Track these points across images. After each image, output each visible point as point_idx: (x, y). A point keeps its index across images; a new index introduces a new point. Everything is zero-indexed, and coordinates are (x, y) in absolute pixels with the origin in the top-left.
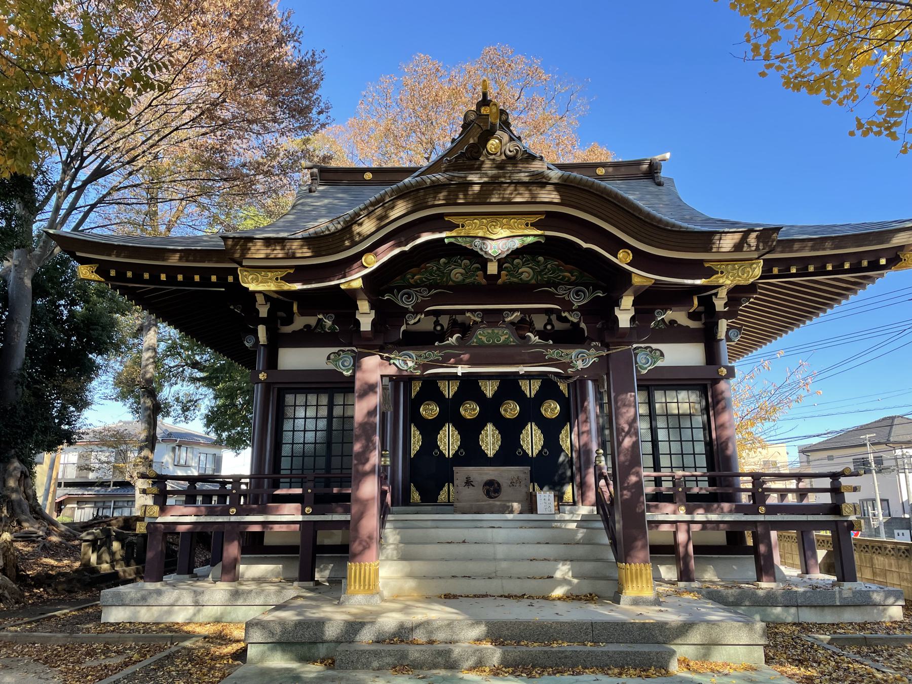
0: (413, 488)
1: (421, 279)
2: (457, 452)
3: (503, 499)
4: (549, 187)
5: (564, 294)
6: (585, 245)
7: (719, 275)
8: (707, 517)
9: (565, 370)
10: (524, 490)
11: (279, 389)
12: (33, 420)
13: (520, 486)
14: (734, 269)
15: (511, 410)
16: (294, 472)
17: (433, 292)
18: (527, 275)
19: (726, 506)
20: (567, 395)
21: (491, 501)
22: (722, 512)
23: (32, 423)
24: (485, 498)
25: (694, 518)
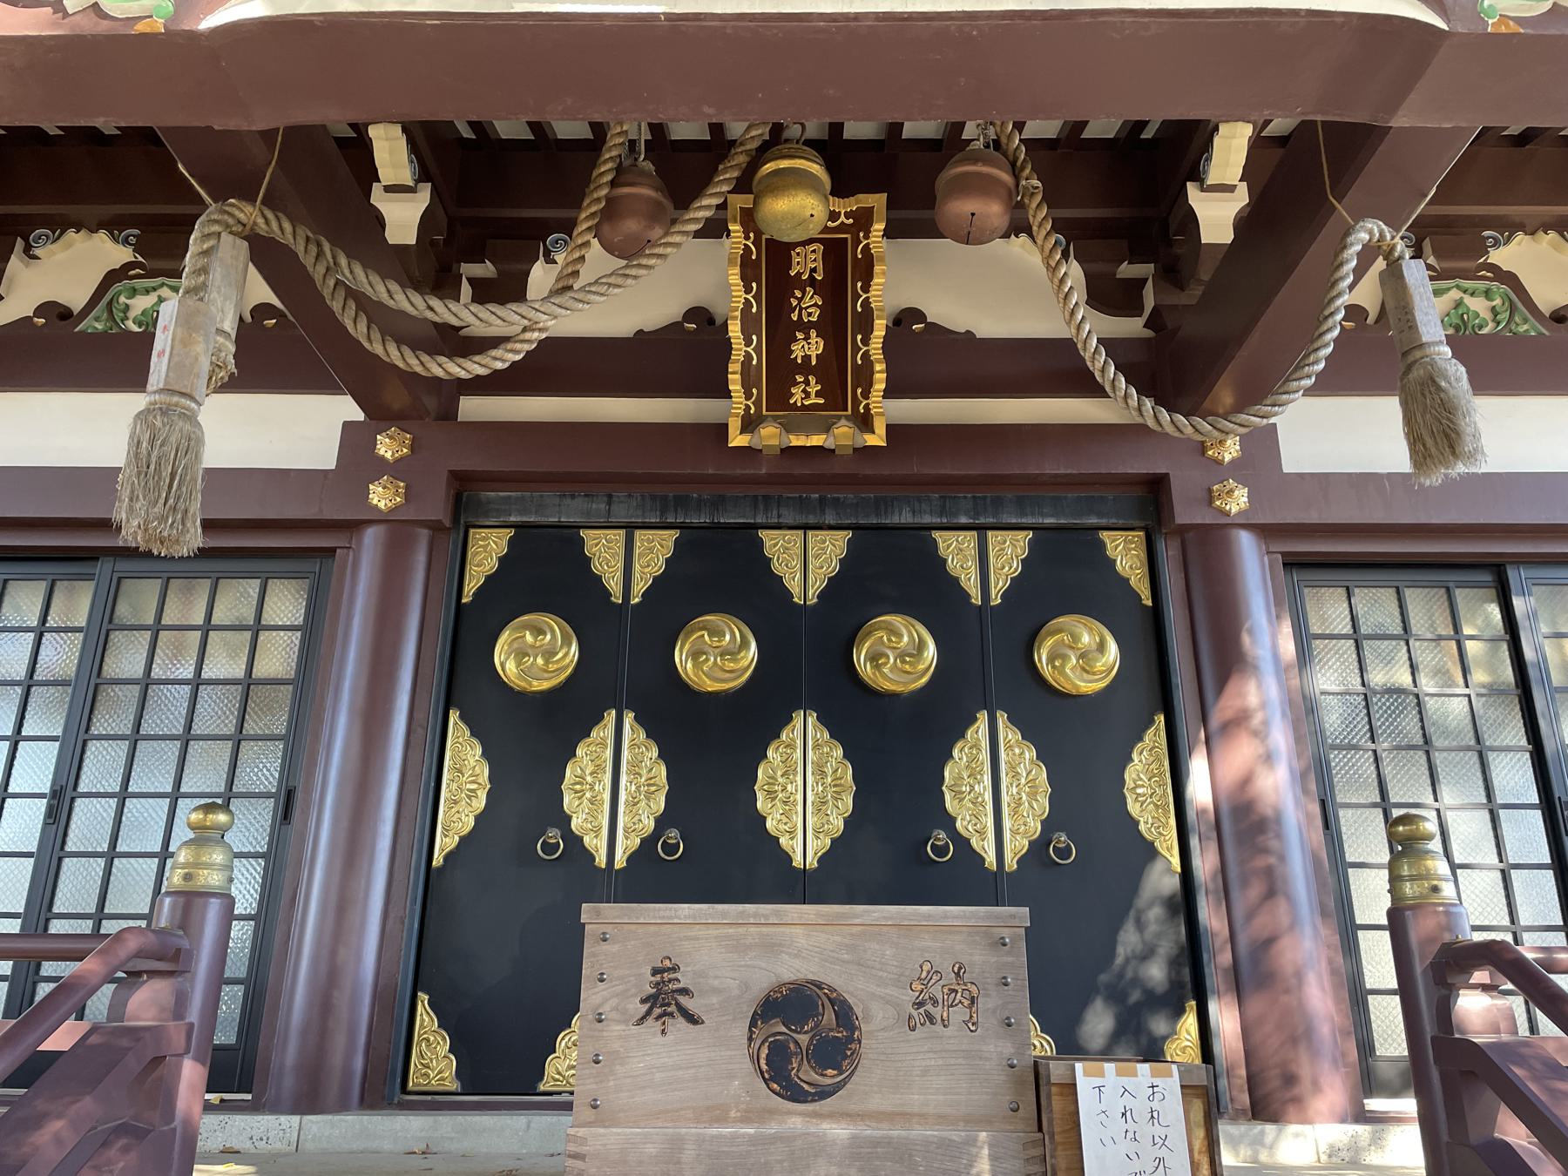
0: (426, 1018)
2: (648, 843)
10: (997, 1048)
13: (971, 1023)
15: (902, 656)
21: (795, 1120)
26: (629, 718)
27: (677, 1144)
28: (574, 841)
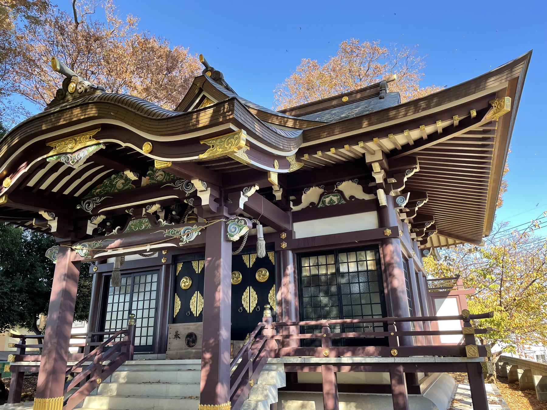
1: (100, 192)
2: (255, 308)
4: (90, 106)
7: (211, 148)
8: (353, 360)
9: (178, 244)
11: (105, 276)
16: (111, 330)
17: (103, 199)
18: (161, 177)
19: (371, 349)
20: (274, 264)
21: (190, 350)
22: (369, 355)
24: (187, 347)
25: (340, 360)
27: (177, 353)
28: (191, 312)
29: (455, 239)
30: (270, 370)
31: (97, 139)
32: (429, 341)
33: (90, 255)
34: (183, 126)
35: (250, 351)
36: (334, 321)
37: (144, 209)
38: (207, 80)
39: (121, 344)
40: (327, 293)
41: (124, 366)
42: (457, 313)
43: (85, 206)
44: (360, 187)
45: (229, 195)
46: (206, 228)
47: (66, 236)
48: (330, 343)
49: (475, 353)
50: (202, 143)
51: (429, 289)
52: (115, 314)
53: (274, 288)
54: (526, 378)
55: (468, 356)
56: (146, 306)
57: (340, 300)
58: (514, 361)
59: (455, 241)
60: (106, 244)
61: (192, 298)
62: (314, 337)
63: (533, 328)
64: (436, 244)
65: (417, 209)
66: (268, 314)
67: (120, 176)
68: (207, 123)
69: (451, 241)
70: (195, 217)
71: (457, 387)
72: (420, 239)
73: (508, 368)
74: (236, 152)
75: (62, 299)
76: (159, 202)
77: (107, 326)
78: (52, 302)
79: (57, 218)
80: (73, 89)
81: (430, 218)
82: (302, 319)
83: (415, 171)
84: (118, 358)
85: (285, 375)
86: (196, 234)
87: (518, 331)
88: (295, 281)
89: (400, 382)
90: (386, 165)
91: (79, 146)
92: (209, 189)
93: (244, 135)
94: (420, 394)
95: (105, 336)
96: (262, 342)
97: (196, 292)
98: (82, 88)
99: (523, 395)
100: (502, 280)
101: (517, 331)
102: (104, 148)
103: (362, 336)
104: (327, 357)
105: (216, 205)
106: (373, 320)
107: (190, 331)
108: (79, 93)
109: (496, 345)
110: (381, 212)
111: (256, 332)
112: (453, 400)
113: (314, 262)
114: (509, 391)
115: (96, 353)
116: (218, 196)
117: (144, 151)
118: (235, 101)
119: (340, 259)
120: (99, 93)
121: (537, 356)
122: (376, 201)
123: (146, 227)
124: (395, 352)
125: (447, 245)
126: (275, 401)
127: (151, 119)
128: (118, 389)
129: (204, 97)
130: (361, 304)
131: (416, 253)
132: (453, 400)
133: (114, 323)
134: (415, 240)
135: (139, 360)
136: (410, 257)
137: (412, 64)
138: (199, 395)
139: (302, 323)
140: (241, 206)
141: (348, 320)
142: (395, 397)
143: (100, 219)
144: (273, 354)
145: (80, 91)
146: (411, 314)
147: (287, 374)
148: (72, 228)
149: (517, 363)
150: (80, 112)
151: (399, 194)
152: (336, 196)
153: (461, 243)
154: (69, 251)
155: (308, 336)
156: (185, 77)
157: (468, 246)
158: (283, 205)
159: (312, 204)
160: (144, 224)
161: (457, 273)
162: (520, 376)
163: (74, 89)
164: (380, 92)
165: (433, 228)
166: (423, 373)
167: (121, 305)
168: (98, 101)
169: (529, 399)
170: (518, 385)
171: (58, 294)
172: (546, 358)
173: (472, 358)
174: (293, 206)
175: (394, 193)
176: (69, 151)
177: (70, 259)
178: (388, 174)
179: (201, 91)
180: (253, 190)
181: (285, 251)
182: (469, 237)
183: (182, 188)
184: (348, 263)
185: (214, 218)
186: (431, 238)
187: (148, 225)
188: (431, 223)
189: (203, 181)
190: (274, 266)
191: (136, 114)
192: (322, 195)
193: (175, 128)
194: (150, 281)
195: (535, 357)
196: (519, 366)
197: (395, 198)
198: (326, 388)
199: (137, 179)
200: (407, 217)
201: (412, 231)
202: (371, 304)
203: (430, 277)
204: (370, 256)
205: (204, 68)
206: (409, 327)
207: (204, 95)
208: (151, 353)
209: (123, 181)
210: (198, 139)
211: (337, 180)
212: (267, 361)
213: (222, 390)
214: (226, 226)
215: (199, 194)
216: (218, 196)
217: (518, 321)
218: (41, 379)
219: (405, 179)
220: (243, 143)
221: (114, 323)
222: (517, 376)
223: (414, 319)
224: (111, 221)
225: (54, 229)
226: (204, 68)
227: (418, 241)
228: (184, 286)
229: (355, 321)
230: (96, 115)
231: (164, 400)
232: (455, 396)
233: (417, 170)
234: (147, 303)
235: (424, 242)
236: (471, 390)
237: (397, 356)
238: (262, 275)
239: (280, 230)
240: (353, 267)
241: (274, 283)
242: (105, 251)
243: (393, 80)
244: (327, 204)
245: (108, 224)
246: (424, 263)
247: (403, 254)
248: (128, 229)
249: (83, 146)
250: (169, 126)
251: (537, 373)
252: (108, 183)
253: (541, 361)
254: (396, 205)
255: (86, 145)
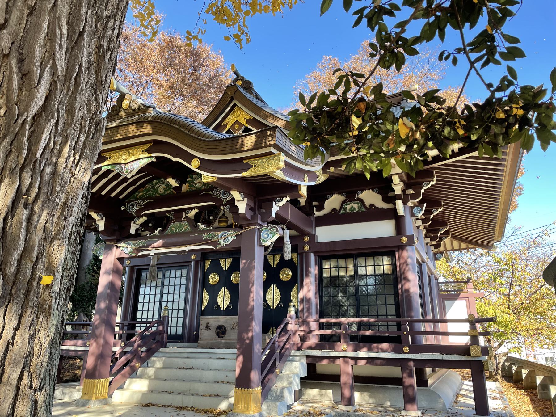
1: (143, 195)
2: (278, 305)
3: (228, 338)
5: (217, 194)
6: (174, 159)
7: (253, 168)
9: (215, 247)
11: (137, 269)
12: (93, 292)
14: (263, 162)
17: (146, 202)
19: (385, 345)
20: (297, 264)
21: (220, 340)
22: (383, 351)
23: (92, 294)
24: (217, 337)
25: (357, 354)
26: (275, 286)
27: (208, 343)
28: (219, 306)
29: (468, 244)
30: (293, 361)
31: (149, 153)
32: (438, 340)
33: (134, 253)
34: (231, 148)
35: (277, 344)
36: (352, 320)
37: (184, 213)
38: (238, 89)
39: (154, 333)
40: (345, 292)
41: (159, 353)
42: (466, 317)
43: (129, 208)
44: (380, 197)
45: (263, 204)
46: (241, 233)
47: (111, 234)
48: (348, 340)
49: (478, 353)
50: (245, 162)
51: (442, 291)
52: (146, 305)
53: (296, 287)
54: (530, 378)
55: (472, 355)
56: (176, 298)
57: (357, 300)
58: (521, 362)
59: (467, 246)
60: (150, 243)
61: (220, 293)
62: (333, 333)
63: (538, 331)
64: (449, 247)
65: (432, 216)
66: (292, 311)
67: (161, 181)
68: (251, 147)
69: (463, 245)
70: (226, 219)
71: (463, 383)
72: (434, 243)
73: (514, 368)
74: (275, 172)
75: (109, 291)
76: (198, 208)
77: (139, 315)
78: (101, 293)
79: (104, 218)
80: (126, 106)
81: (444, 224)
82: (321, 317)
83: (432, 183)
84: (154, 346)
85: (306, 366)
86: (233, 238)
87: (524, 333)
88: (316, 281)
89: (411, 376)
90: (405, 178)
91: (133, 158)
92: (246, 199)
93: (283, 157)
94: (428, 386)
95: (137, 325)
96: (287, 336)
97: (223, 287)
98: (135, 105)
99: (526, 394)
100: (511, 284)
101: (523, 334)
102: (155, 160)
103: (378, 334)
104: (346, 351)
105: (252, 213)
106: (387, 320)
107: (220, 324)
108: (132, 110)
109: (503, 347)
110: (399, 221)
111: (282, 326)
112: (458, 395)
113: (334, 264)
114: (513, 390)
115: (136, 340)
116: (253, 206)
117: (192, 166)
118: (277, 129)
119: (358, 263)
120: (151, 112)
121: (546, 358)
122: (395, 210)
123: (185, 230)
124: (406, 349)
125: (460, 249)
126: (298, 388)
127: (201, 140)
128: (155, 373)
129: (235, 105)
130: (377, 305)
131: (429, 258)
132: (458, 395)
133: (145, 313)
134: (429, 245)
135: (172, 348)
136: (423, 262)
137: (433, 64)
138: (234, 381)
139: (323, 320)
140: (273, 215)
141: (365, 319)
142: (406, 389)
143: (142, 220)
144: (295, 348)
145: (133, 108)
146: (423, 317)
147: (309, 365)
148: (116, 228)
149: (522, 364)
150: (135, 129)
151: (417, 204)
152: (357, 204)
153: (473, 248)
154: (115, 248)
155: (328, 332)
156: (210, 76)
157: (479, 251)
158: (307, 211)
159: (334, 210)
160: (184, 226)
161: (469, 275)
162: (524, 376)
163: (128, 106)
164: (402, 102)
165: (447, 233)
166: (431, 369)
167: (152, 297)
168: (152, 120)
169: (531, 397)
170: (522, 384)
171: (106, 286)
172: (555, 360)
173: (475, 357)
174: (317, 211)
175: (411, 203)
176: (123, 162)
177: (115, 256)
178: (407, 186)
179: (232, 99)
180: (284, 201)
181: (307, 253)
182: (481, 242)
183: (219, 196)
184: (366, 266)
185: (249, 225)
186: (444, 243)
187: (187, 228)
188: (445, 229)
189: (241, 192)
190: (297, 267)
191: (187, 134)
192: (343, 203)
193: (224, 149)
194: (180, 276)
195: (544, 359)
196: (524, 367)
197: (412, 208)
198: (344, 379)
199: (178, 185)
200: (423, 223)
201: (426, 236)
202: (386, 305)
203: (441, 279)
204: (386, 261)
205: (235, 76)
206: (420, 328)
207: (235, 103)
208: (180, 342)
209: (164, 186)
210: (241, 160)
211: (358, 189)
212: (290, 353)
213: (255, 376)
214: (260, 233)
215: (236, 203)
216: (253, 206)
217: (524, 324)
218: (90, 362)
219: (422, 191)
220: (282, 165)
221: (145, 313)
222: (522, 376)
223: (425, 321)
224: (153, 222)
225: (101, 228)
226: (235, 76)
227: (432, 245)
228: (212, 282)
229: (372, 320)
230: (150, 132)
231: (199, 384)
232: (460, 391)
233: (435, 182)
234: (176, 296)
235: (437, 246)
236: (473, 386)
237: (408, 353)
238: (286, 275)
239: (303, 234)
240: (370, 270)
241: (297, 282)
242: (148, 250)
243: (415, 90)
244: (348, 211)
245: (150, 225)
246: (437, 265)
247: (417, 260)
248: (169, 230)
249: (136, 158)
250: (218, 147)
251: (540, 373)
252: (150, 187)
253: (550, 364)
254: (413, 215)
255: (139, 158)
